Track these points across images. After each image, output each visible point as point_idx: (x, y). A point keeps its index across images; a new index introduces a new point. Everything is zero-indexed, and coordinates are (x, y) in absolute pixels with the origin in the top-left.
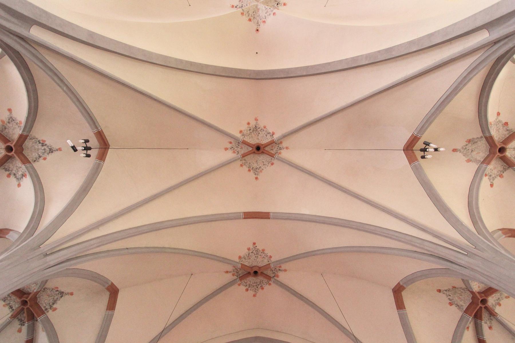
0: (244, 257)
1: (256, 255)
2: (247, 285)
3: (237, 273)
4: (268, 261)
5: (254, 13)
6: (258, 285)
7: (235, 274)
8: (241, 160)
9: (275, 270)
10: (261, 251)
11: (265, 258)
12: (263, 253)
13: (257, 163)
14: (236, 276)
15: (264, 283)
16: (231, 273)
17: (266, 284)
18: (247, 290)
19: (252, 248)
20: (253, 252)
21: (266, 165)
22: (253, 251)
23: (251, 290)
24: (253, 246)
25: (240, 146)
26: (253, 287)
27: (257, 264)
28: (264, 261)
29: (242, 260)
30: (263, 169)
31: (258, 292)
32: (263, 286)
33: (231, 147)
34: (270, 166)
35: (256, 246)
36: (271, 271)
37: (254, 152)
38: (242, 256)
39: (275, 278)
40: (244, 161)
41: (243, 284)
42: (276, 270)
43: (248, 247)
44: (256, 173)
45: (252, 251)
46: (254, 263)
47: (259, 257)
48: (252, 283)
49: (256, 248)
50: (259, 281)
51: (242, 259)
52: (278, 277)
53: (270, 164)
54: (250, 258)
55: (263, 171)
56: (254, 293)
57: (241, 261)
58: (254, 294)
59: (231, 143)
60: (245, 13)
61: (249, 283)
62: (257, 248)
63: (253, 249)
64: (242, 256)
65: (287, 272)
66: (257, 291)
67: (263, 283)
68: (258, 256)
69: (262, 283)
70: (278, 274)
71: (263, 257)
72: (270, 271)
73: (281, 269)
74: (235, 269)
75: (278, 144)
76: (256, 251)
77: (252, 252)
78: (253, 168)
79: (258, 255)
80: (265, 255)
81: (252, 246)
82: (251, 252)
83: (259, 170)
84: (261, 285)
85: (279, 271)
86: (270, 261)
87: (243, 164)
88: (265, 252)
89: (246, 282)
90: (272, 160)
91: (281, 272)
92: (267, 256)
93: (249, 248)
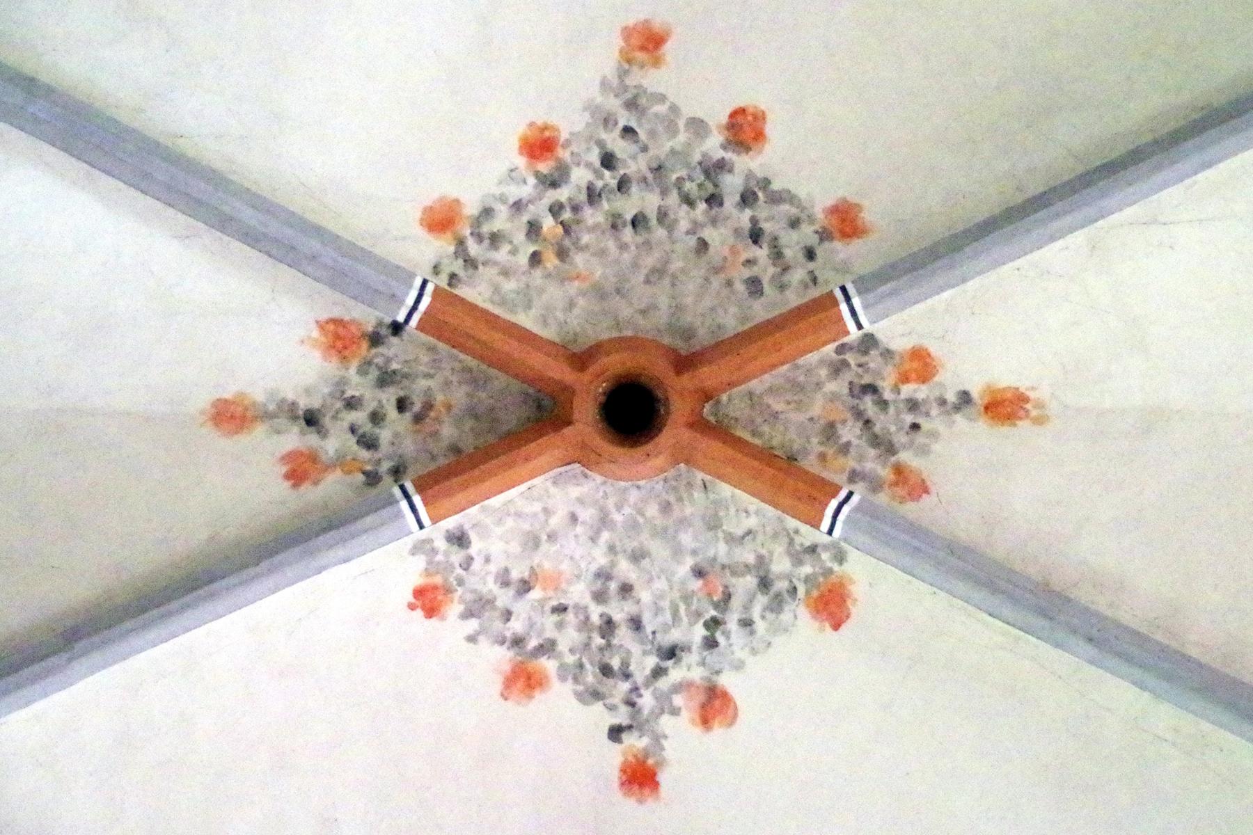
0: (777, 604)
1: (619, 611)
2: (747, 199)
3: (871, 389)
4: (459, 539)
6: (593, 195)
7: (905, 379)
9: (376, 418)
10: (548, 665)
12: (533, 643)
14: (888, 354)
15: (520, 237)
16: (951, 380)
17: (487, 212)
20: (652, 661)
22: (658, 672)
23: (698, 126)
24: (658, 738)
26: (658, 169)
27: (611, 503)
28: (515, 547)
29: (807, 569)
32: (527, 189)
35: (616, 733)
36: (428, 406)
37: (684, 363)
38: (800, 617)
39: (367, 317)
41: (794, 224)
42: (359, 417)
43: (718, 732)
45: (676, 674)
46: (652, 510)
47: (579, 593)
48: (683, 217)
49: (622, 717)
50: (579, 259)
51: (807, 579)
52: (337, 322)
54: (697, 584)
56: (652, 80)
57: (813, 549)
61: (709, 234)
62: (600, 717)
63: (659, 697)
64: (803, 612)
65: (202, 400)
66: (614, 104)
67: (533, 229)
69: (548, 223)
70: (332, 367)
71: (525, 587)
72: (440, 398)
73: (294, 439)
74: (901, 438)
76: (615, 663)
77: (671, 653)
79: (595, 613)
80: (507, 615)
81: (671, 749)
84: (563, 194)
85: (315, 403)
86: (441, 544)
89: (762, 253)
91: (290, 396)
92: (478, 607)
93: (706, 721)
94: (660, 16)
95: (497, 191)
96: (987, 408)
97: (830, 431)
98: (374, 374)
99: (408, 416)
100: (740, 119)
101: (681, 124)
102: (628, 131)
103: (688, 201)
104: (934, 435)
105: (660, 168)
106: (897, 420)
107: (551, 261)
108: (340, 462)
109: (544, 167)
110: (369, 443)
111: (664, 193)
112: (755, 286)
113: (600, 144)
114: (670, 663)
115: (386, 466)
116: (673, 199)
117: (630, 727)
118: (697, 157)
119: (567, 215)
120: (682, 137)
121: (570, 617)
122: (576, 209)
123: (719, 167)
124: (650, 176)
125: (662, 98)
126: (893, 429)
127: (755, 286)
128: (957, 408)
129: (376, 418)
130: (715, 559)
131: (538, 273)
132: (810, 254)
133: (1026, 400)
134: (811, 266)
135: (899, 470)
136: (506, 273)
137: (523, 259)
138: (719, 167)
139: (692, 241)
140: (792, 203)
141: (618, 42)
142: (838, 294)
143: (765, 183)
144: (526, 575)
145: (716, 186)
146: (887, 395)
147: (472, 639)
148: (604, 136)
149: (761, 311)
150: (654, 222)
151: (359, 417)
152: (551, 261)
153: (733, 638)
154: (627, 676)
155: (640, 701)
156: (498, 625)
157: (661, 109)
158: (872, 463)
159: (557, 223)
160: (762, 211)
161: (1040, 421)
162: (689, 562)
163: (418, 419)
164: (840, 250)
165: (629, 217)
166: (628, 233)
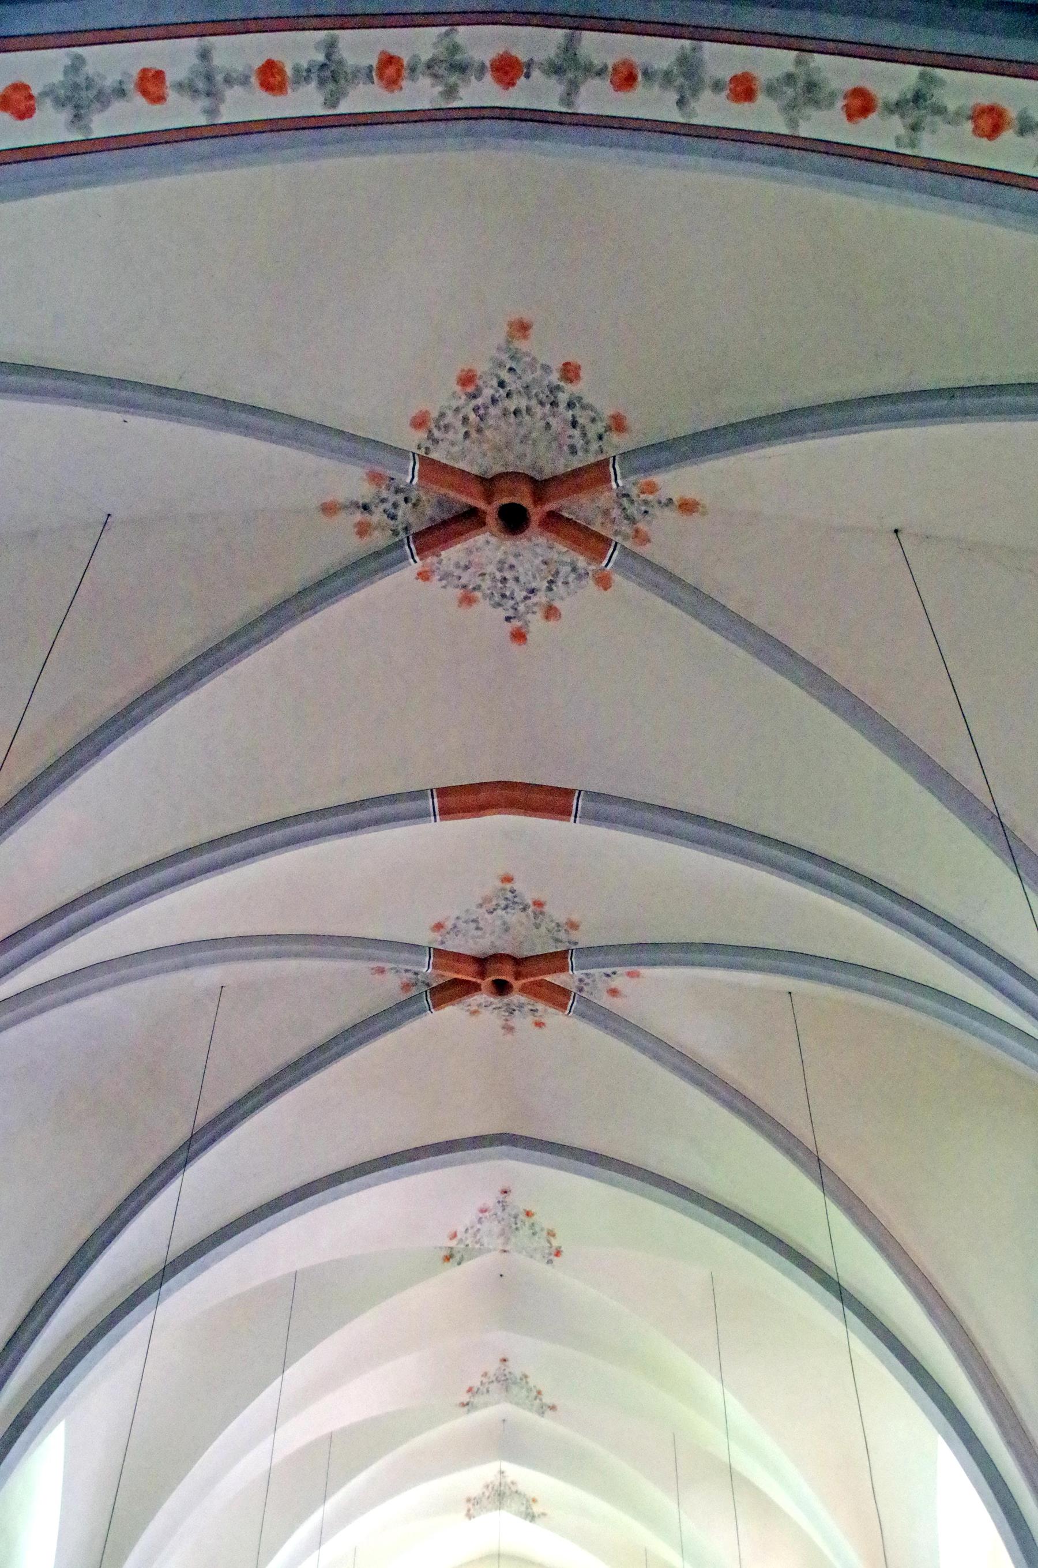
1: (508, 575)
2: (570, 405)
5: (514, 1226)
6: (494, 401)
8: (576, 943)
9: (395, 505)
10: (478, 594)
11: (457, 565)
13: (504, 923)
15: (458, 424)
16: (664, 494)
17: (442, 415)
18: (570, 372)
19: (529, 617)
20: (524, 593)
21: (466, 922)
22: (526, 598)
23: (546, 369)
24: (527, 623)
25: (576, 979)
30: (481, 906)
31: (494, 352)
33: (613, 976)
34: (447, 918)
38: (590, 583)
40: (562, 935)
41: (593, 420)
42: (388, 506)
43: (552, 623)
44: (509, 895)
45: (535, 599)
47: (491, 569)
48: (539, 411)
49: (510, 613)
50: (488, 433)
53: (449, 925)
54: (544, 567)
55: (480, 901)
56: (522, 345)
58: (525, 337)
59: (614, 992)
60: (545, 1233)
61: (551, 420)
62: (501, 613)
64: (591, 582)
65: (316, 503)
66: (505, 357)
67: (465, 420)
68: (500, 570)
71: (467, 568)
73: (358, 516)
75: (420, 984)
76: (508, 593)
77: (532, 591)
78: (524, 909)
79: (498, 575)
80: (460, 578)
81: (532, 628)
82: (539, 594)
83: (494, 903)
84: (479, 401)
85: (366, 500)
87: (566, 927)
88: (459, 592)
89: (577, 433)
90: (440, 938)
94: (527, 316)
95: (446, 404)
96: (680, 506)
97: (606, 513)
98: (392, 489)
99: (410, 505)
100: (569, 367)
101: (538, 366)
102: (511, 369)
103: (542, 403)
104: (654, 516)
105: (527, 387)
106: (638, 510)
107: (474, 435)
108: (379, 526)
109: (471, 389)
110: (393, 517)
111: (529, 398)
112: (573, 450)
113: (498, 376)
114: (532, 595)
115: (400, 527)
116: (534, 402)
117: (515, 617)
118: (546, 383)
119: (482, 411)
120: (539, 372)
121: (487, 577)
122: (486, 408)
123: (554, 389)
124: (522, 391)
125: (527, 354)
126: (636, 512)
127: (573, 450)
128: (667, 505)
129: (395, 505)
130: (552, 559)
131: (468, 442)
132: (600, 437)
133: (698, 504)
134: (601, 443)
135: (637, 531)
136: (453, 444)
137: (461, 436)
138: (554, 389)
139: (543, 423)
140: (592, 410)
141: (506, 328)
142: (613, 544)
143: (580, 399)
144: (467, 563)
145: (555, 397)
146: (635, 498)
147: (444, 587)
148: (499, 372)
149: (576, 463)
150: (524, 412)
151: (388, 506)
152: (474, 435)
153: (559, 588)
154: (512, 598)
155: (519, 608)
156: (456, 582)
157: (528, 359)
158: (626, 528)
159: (476, 415)
160: (577, 411)
161: (704, 514)
162: (541, 558)
163: (414, 505)
164: (614, 438)
165: (512, 410)
166: (512, 418)
